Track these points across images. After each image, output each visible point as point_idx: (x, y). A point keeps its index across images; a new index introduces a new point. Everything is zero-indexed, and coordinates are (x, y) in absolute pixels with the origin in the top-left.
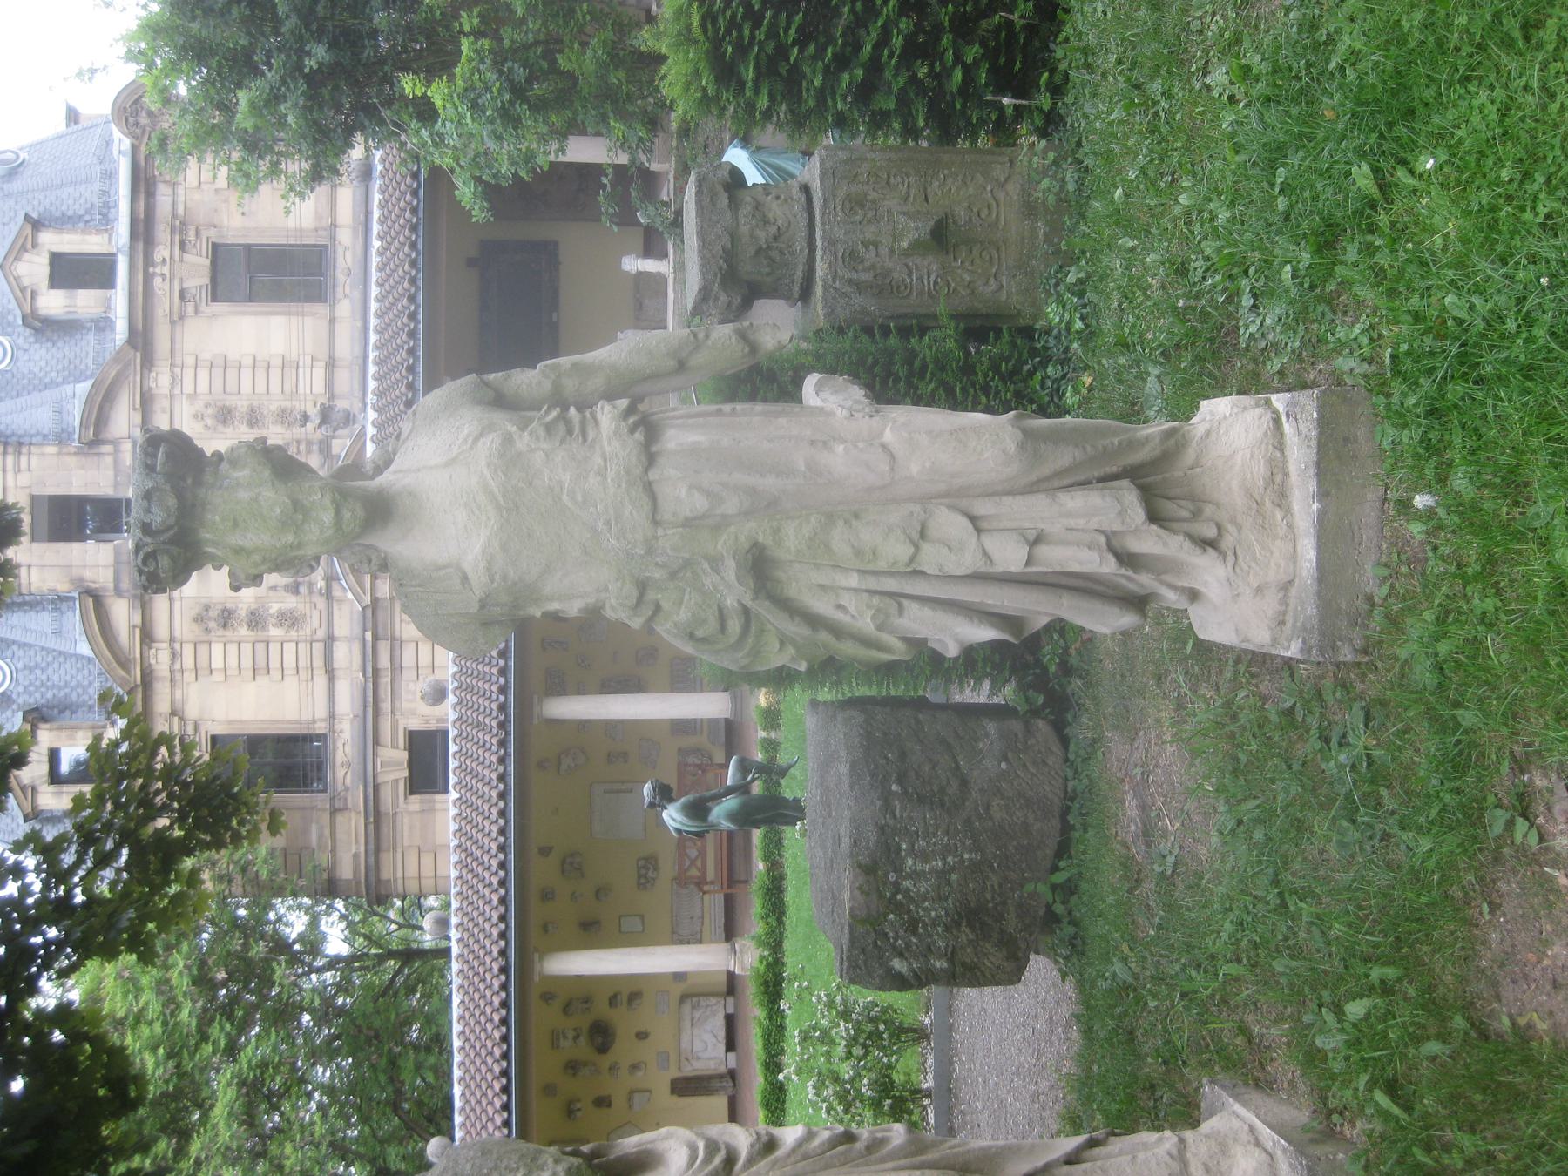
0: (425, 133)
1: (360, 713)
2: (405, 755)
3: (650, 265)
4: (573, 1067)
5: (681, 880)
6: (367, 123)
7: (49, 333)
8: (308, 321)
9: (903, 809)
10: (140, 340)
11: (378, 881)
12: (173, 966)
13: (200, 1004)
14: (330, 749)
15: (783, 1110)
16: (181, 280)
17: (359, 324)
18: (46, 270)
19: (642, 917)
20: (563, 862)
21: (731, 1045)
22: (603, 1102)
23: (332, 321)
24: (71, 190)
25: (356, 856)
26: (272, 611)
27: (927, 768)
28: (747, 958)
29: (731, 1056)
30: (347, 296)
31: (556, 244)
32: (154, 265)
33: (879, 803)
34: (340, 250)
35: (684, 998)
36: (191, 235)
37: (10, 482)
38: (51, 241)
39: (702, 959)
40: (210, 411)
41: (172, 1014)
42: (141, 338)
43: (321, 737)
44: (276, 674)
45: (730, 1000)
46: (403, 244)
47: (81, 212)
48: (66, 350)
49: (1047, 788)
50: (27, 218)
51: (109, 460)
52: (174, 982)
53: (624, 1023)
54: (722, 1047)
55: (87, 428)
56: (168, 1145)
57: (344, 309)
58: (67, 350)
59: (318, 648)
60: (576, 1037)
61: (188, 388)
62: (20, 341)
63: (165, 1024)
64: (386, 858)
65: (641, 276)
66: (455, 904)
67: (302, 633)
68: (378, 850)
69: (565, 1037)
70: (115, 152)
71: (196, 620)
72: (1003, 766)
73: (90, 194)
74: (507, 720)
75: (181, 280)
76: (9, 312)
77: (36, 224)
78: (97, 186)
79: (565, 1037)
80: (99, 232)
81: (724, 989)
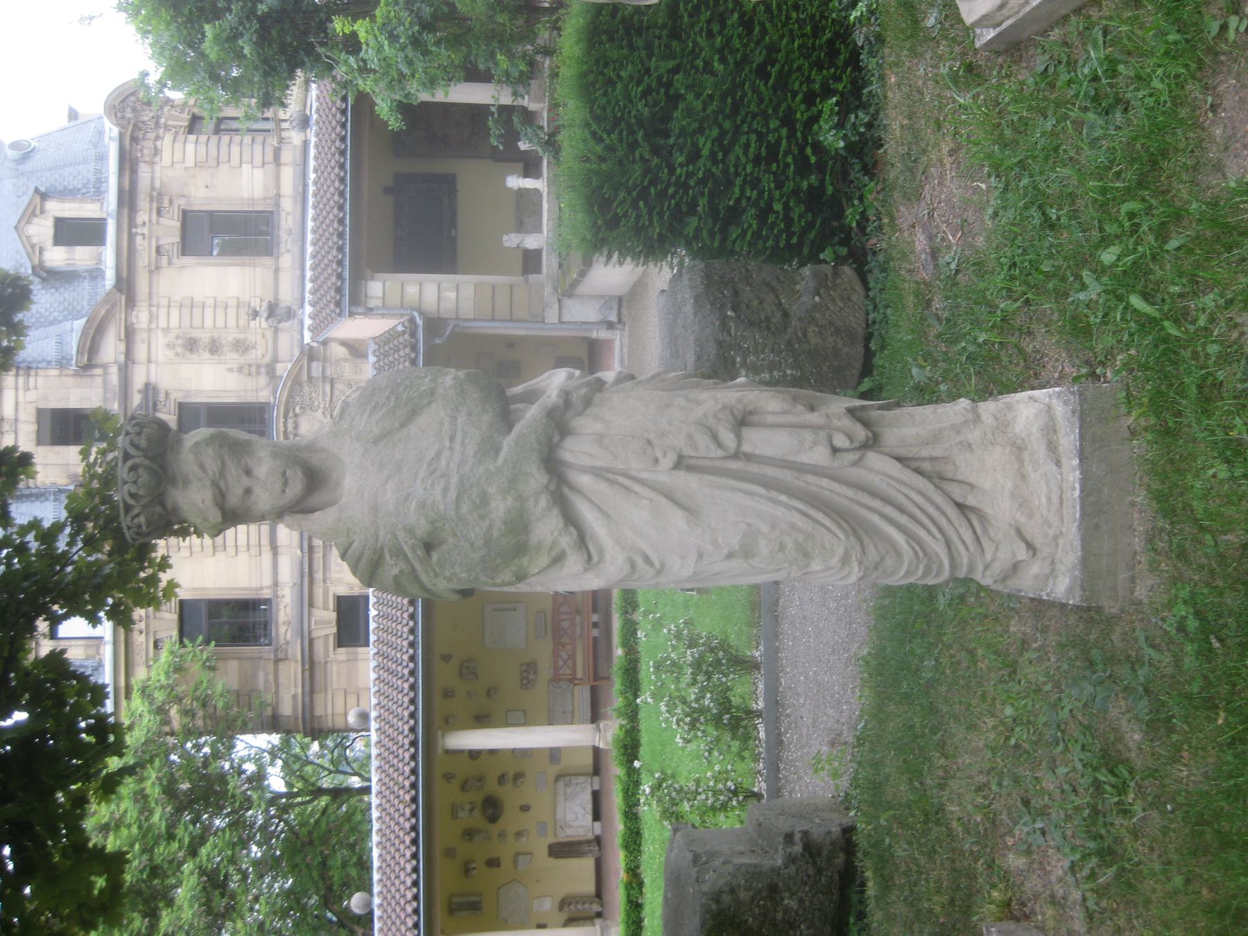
0: (352, 60)
1: (297, 580)
2: (334, 616)
3: (529, 183)
4: (469, 834)
5: (556, 679)
6: (306, 59)
8: (258, 270)
9: (737, 329)
10: (124, 286)
11: (312, 717)
12: (148, 778)
13: (168, 809)
14: (274, 611)
15: (639, 851)
16: (158, 239)
17: (298, 273)
18: (51, 231)
19: (524, 712)
20: (461, 666)
21: (597, 816)
22: (493, 863)
23: (277, 270)
24: (71, 169)
25: (295, 697)
27: (755, 303)
28: (608, 734)
29: (597, 824)
30: (288, 251)
31: (454, 175)
32: (136, 227)
33: (717, 323)
34: (283, 215)
35: (558, 778)
36: (166, 203)
37: (21, 398)
38: (57, 208)
39: (570, 736)
40: (180, 341)
42: (126, 284)
43: (267, 601)
44: (231, 551)
45: (596, 779)
46: (332, 208)
47: (80, 186)
48: (66, 295)
49: (852, 319)
50: (37, 190)
51: (99, 380)
52: (148, 791)
53: (511, 797)
54: (590, 817)
55: (82, 354)
56: (142, 923)
57: (286, 261)
58: (67, 294)
60: (472, 810)
61: (163, 323)
63: (140, 827)
64: (319, 698)
65: (522, 193)
68: (312, 692)
69: (463, 809)
70: (107, 139)
72: (817, 299)
73: (87, 172)
75: (158, 239)
76: (21, 266)
77: (44, 196)
78: (92, 166)
79: (463, 809)
80: (93, 201)
81: (591, 769)
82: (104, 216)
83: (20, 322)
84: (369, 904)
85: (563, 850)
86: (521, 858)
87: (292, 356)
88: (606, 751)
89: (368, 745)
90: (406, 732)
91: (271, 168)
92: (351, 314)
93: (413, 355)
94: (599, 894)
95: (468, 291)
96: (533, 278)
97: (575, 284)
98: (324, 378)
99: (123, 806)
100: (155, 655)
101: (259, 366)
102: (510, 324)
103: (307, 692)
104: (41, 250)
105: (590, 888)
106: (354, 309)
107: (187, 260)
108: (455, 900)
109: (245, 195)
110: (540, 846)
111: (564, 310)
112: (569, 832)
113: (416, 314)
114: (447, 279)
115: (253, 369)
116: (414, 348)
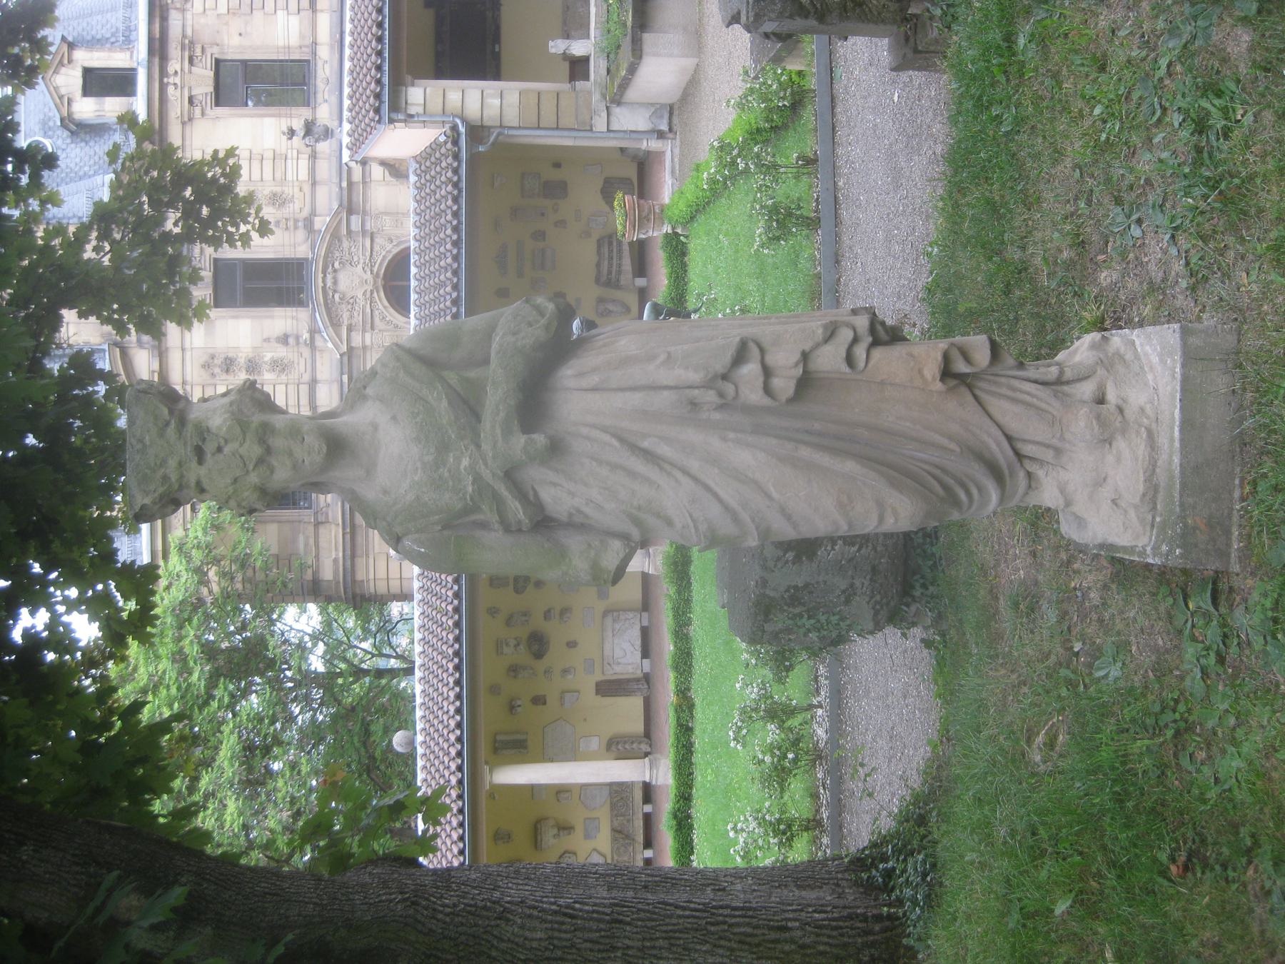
4: (514, 670)
7: (82, 135)
11: (354, 581)
15: (690, 673)
16: (190, 88)
18: (80, 82)
21: (646, 653)
22: (539, 700)
24: (99, 17)
25: (336, 561)
26: (266, 359)
29: (646, 662)
30: (326, 101)
35: (606, 613)
36: (198, 52)
41: (186, 680)
45: (645, 615)
47: (108, 35)
48: (97, 148)
52: (187, 650)
54: (638, 654)
59: (304, 389)
62: (59, 142)
63: (179, 689)
64: (360, 562)
66: (418, 636)
67: (291, 377)
68: (353, 556)
69: (507, 644)
71: (203, 366)
73: (116, 20)
74: (460, 223)
75: (190, 88)
76: (50, 119)
78: (120, 14)
79: (507, 644)
80: (122, 50)
81: (640, 606)
82: (134, 65)
83: (45, 38)
84: (411, 743)
85: (611, 688)
86: (568, 696)
87: (331, 210)
88: (658, 577)
89: (412, 642)
90: (451, 670)
91: (307, 14)
92: (391, 121)
93: (455, 164)
94: (648, 734)
95: (513, 98)
96: (580, 84)
97: (625, 85)
98: (364, 232)
99: (161, 667)
100: (192, 519)
101: (296, 221)
102: (556, 133)
103: (348, 557)
104: (70, 101)
105: (640, 728)
106: (394, 116)
107: (220, 111)
108: (499, 738)
109: (281, 43)
110: (587, 684)
111: (613, 118)
112: (618, 669)
113: (458, 121)
114: (491, 86)
115: (291, 223)
116: (456, 157)
